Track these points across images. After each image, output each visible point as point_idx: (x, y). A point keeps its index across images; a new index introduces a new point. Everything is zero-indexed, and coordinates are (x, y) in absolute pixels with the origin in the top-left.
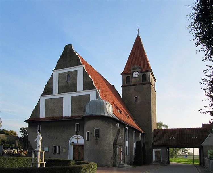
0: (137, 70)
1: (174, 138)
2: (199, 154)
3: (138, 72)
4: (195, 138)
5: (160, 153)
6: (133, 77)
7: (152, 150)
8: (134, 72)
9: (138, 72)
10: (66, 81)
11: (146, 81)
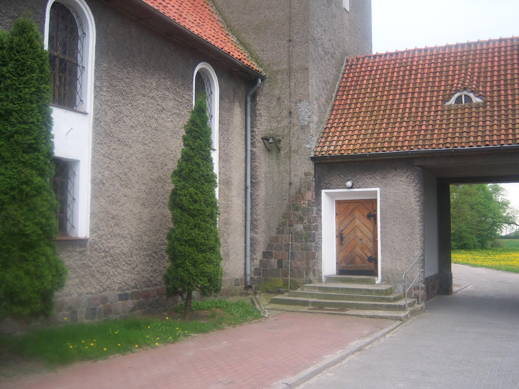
1: (476, 100)
2: (454, 196)
4: (468, 99)
5: (372, 217)
7: (309, 195)
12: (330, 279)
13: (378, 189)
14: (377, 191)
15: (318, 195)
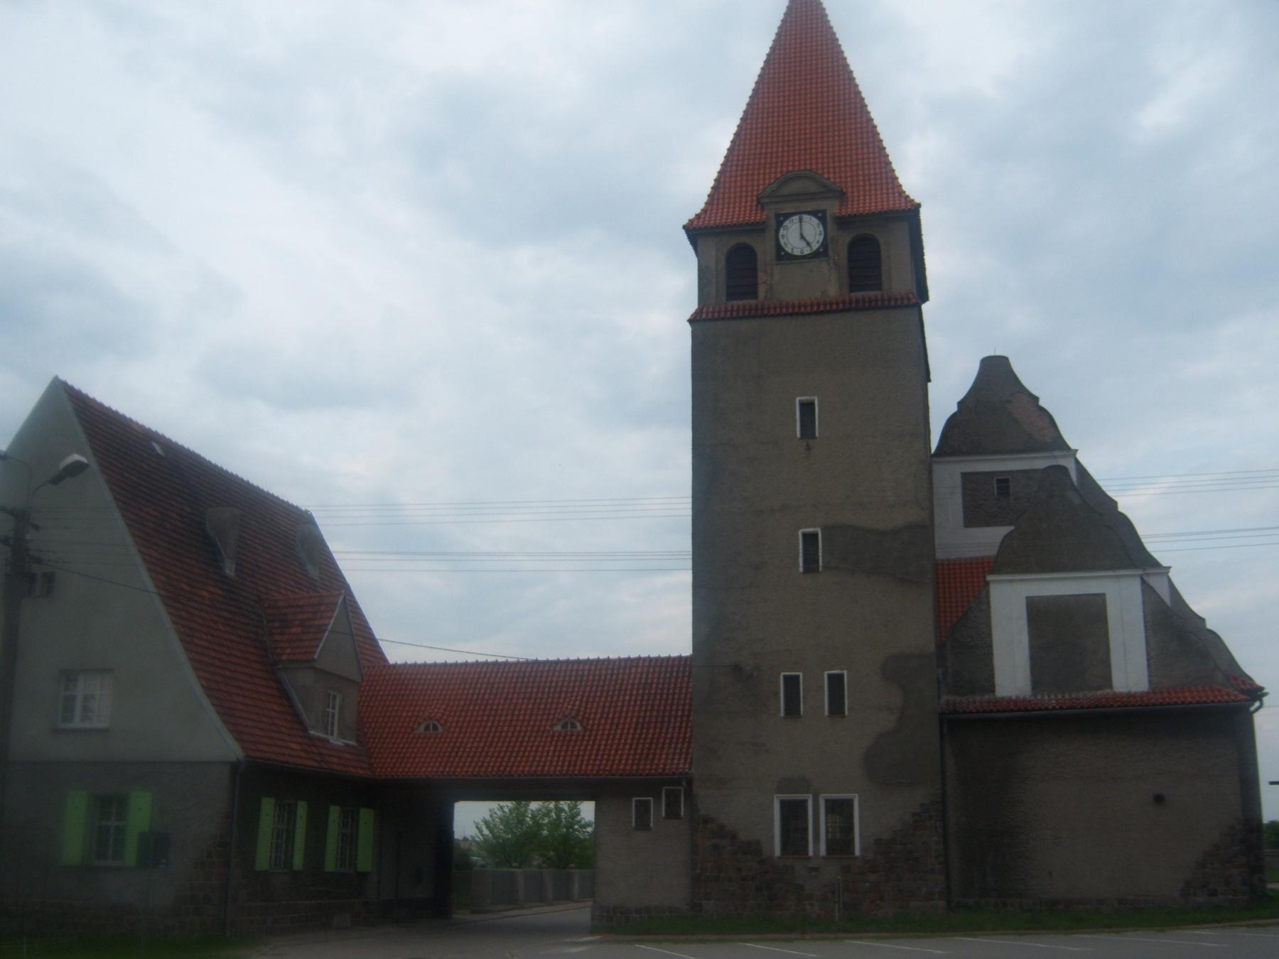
0: (811, 206)
3: (823, 220)
6: (782, 256)
8: (787, 216)
9: (820, 215)
11: (878, 286)
12: (779, 858)
13: (651, 799)
15: (773, 798)
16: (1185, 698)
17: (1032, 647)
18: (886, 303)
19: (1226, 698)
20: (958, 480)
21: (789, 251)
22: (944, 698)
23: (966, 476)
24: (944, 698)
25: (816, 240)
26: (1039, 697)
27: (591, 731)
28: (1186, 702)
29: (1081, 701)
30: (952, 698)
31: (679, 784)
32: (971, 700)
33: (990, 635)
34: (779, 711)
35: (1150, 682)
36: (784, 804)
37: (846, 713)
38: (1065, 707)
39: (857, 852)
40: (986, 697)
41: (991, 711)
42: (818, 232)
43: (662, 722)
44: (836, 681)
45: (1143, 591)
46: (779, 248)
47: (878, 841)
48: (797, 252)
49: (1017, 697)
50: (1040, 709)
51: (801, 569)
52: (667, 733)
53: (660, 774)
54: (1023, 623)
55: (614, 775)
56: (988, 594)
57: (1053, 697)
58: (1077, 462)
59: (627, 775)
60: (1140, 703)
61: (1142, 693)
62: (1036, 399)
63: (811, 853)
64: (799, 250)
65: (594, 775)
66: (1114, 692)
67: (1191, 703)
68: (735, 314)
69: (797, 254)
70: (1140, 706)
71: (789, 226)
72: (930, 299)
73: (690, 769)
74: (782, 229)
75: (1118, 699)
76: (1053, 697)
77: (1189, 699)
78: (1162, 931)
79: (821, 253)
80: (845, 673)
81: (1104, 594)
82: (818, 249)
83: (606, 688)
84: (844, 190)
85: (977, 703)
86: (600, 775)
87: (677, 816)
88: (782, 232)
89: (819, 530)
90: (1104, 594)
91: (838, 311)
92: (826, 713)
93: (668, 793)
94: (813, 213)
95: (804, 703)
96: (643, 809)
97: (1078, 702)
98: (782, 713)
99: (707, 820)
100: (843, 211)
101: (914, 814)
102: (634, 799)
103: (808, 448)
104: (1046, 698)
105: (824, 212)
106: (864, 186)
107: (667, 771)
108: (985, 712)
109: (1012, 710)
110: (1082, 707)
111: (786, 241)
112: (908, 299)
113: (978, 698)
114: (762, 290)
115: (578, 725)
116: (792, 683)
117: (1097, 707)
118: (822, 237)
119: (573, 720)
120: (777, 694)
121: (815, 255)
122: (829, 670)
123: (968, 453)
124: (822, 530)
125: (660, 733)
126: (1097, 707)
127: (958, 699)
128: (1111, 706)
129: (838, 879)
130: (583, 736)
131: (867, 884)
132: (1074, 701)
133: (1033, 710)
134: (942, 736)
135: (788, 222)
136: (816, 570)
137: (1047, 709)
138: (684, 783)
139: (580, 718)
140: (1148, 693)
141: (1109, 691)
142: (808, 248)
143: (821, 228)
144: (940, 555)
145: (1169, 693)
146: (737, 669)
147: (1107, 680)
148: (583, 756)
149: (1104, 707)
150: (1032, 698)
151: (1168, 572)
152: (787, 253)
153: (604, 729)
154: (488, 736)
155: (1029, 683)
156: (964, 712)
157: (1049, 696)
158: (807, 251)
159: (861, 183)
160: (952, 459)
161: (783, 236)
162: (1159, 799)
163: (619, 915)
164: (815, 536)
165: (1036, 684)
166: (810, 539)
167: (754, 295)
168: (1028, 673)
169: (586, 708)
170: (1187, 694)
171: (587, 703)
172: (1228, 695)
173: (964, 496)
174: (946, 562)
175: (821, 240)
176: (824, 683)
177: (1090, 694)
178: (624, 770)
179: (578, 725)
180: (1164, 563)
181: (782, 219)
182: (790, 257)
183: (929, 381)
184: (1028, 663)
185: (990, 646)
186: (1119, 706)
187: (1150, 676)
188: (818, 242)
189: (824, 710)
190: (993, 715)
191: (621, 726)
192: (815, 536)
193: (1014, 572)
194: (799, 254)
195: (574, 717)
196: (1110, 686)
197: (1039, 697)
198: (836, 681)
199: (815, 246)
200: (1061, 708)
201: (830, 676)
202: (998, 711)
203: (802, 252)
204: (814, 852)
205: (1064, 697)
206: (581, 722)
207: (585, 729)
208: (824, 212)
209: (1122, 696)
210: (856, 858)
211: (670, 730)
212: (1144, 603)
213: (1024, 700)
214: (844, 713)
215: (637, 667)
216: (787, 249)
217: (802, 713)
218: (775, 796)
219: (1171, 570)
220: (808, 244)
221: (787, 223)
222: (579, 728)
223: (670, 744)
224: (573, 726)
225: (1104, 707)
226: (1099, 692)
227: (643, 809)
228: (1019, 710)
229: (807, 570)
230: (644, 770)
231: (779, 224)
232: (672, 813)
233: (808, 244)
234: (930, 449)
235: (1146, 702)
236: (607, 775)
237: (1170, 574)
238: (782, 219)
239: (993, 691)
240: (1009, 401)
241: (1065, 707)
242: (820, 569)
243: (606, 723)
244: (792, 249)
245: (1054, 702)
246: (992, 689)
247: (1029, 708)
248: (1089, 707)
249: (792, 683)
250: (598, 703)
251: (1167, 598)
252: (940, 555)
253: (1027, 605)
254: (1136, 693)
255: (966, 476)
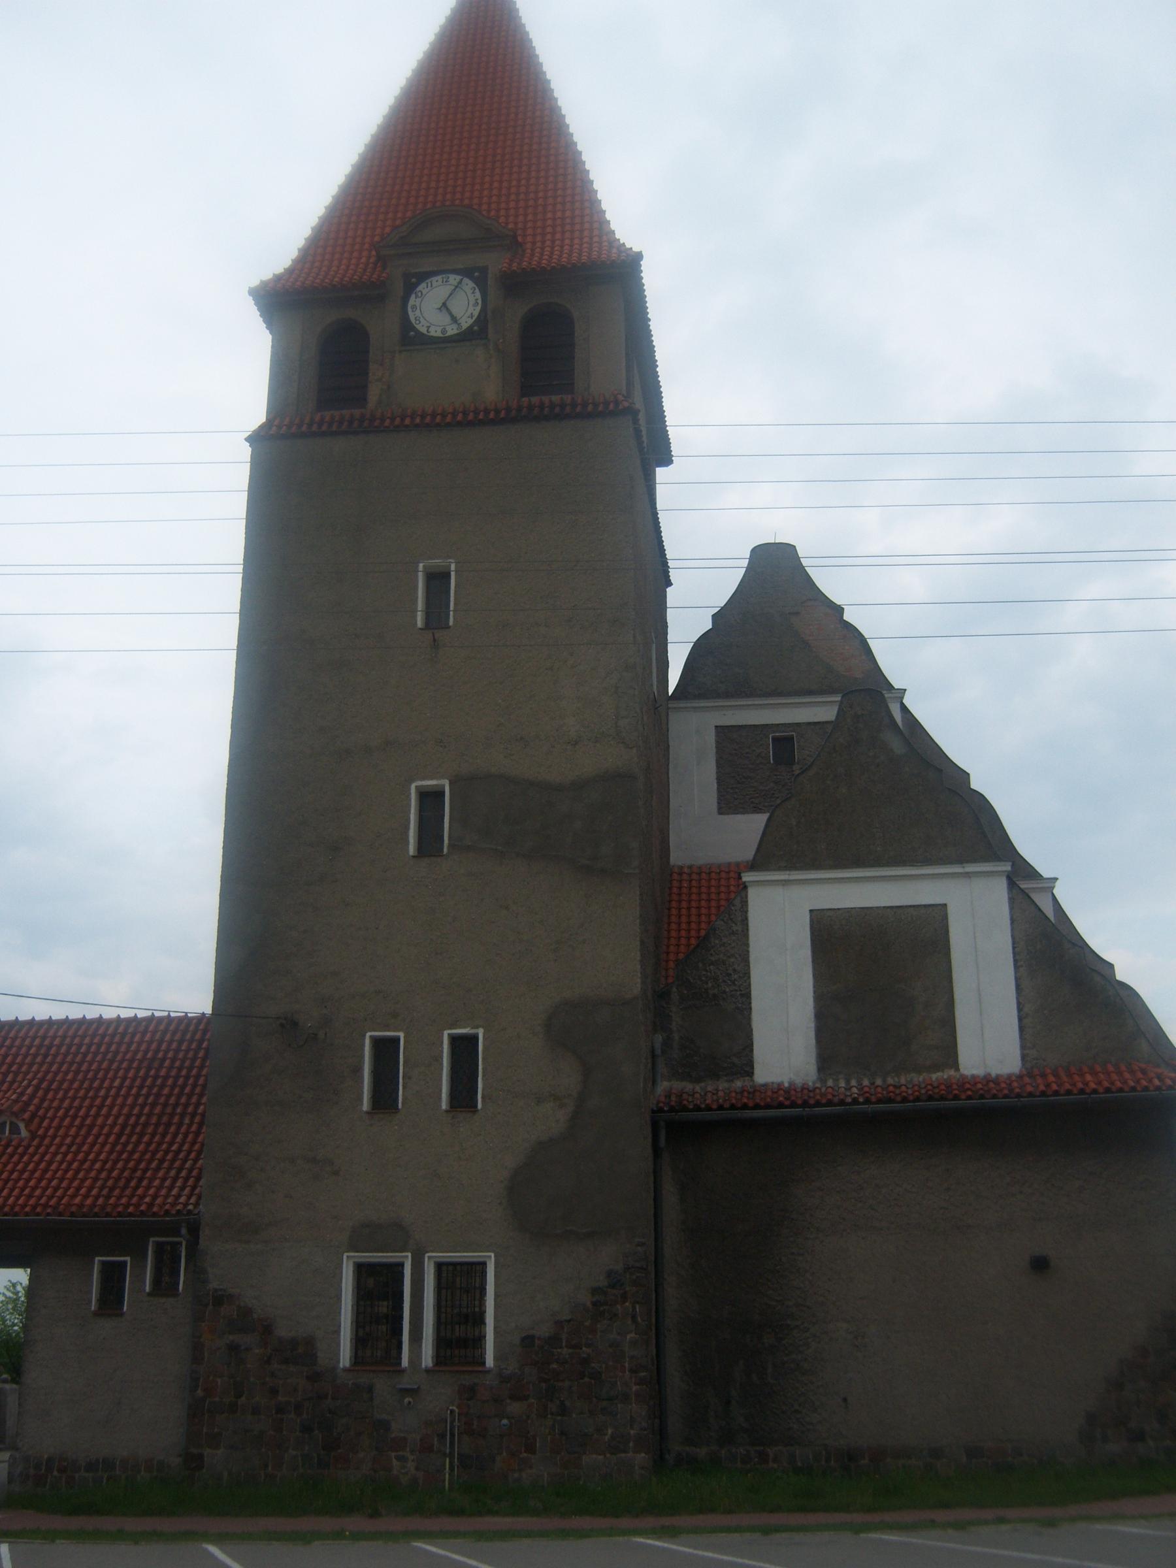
3: (481, 283)
6: (411, 338)
8: (424, 276)
9: (478, 276)
10: (420, 622)
12: (345, 1370)
13: (128, 1259)
14: (125, 1262)
16: (1087, 1084)
17: (819, 997)
18: (579, 409)
19: (1157, 1082)
20: (711, 738)
21: (423, 330)
22: (663, 1086)
23: (723, 732)
24: (663, 1086)
25: (469, 313)
26: (830, 1083)
27: (43, 1137)
28: (1088, 1091)
29: (903, 1088)
30: (678, 1085)
31: (177, 1233)
32: (709, 1089)
33: (747, 975)
34: (360, 1099)
35: (1024, 1057)
36: (362, 1270)
37: (480, 1106)
38: (873, 1099)
39: (490, 1361)
40: (738, 1084)
41: (745, 1107)
42: (472, 301)
43: (169, 1124)
44: (464, 1048)
45: (1012, 900)
46: (406, 325)
47: (528, 1341)
48: (435, 332)
49: (791, 1084)
50: (830, 1103)
51: (412, 850)
52: (171, 1144)
53: (143, 1213)
54: (805, 953)
55: (60, 1214)
56: (745, 903)
57: (854, 1083)
58: (904, 709)
59: (84, 1216)
60: (1006, 1092)
61: (1010, 1076)
62: (839, 610)
63: (405, 1362)
64: (439, 330)
65: (27, 1214)
66: (963, 1077)
67: (1095, 1091)
68: (324, 428)
69: (435, 335)
70: (1006, 1096)
71: (424, 292)
72: (676, 447)
73: (196, 1205)
74: (413, 296)
75: (968, 1086)
76: (854, 1083)
77: (1092, 1085)
78: (1051, 1523)
79: (475, 334)
80: (481, 1033)
81: (945, 905)
82: (471, 327)
83: (84, 1068)
84: (520, 239)
85: (721, 1094)
86: (38, 1214)
87: (172, 1290)
88: (412, 301)
89: (446, 784)
90: (945, 905)
91: (493, 422)
92: (444, 1105)
93: (160, 1249)
94: (467, 273)
95: (404, 1087)
96: (113, 1279)
97: (898, 1092)
98: (366, 1105)
99: (220, 1299)
100: (515, 264)
101: (595, 1291)
102: (97, 1259)
103: (435, 642)
104: (842, 1084)
105: (484, 270)
106: (553, 234)
107: (155, 1209)
108: (733, 1107)
109: (781, 1105)
110: (905, 1100)
111: (418, 305)
112: (617, 402)
113: (723, 1085)
114: (374, 393)
115: (22, 1126)
116: (385, 1050)
117: (930, 1098)
118: (478, 308)
119: (14, 1119)
120: (358, 1070)
121: (466, 337)
122: (450, 1029)
123: (728, 695)
124: (451, 784)
125: (160, 1144)
126: (930, 1098)
127: (688, 1086)
128: (956, 1098)
129: (452, 1411)
130: (27, 1147)
131: (505, 1421)
132: (891, 1088)
133: (818, 1104)
134: (657, 1152)
135: (423, 285)
136: (438, 853)
137: (842, 1103)
138: (184, 1231)
139: (26, 1115)
140: (1020, 1077)
141: (952, 1072)
142: (455, 326)
143: (478, 295)
144: (677, 857)
145: (1056, 1075)
146: (289, 1025)
147: (949, 1052)
148: (17, 1181)
149: (942, 1098)
150: (818, 1085)
151: (1053, 888)
152: (417, 284)
153: (66, 1135)
154: (74, 1178)
155: (813, 1060)
156: (698, 1109)
157: (848, 1081)
158: (452, 330)
159: (549, 229)
160: (703, 703)
161: (414, 307)
162: (1040, 1264)
163: (55, 1473)
164: (438, 794)
165: (826, 1060)
166: (430, 799)
167: (362, 400)
168: (813, 1041)
169: (43, 1100)
170: (1088, 1077)
171: (47, 1091)
172: (1159, 1077)
173: (719, 765)
174: (686, 870)
175: (476, 313)
176: (442, 1052)
177: (918, 1078)
178: (81, 1206)
179: (22, 1126)
180: (1046, 873)
181: (414, 280)
182: (424, 341)
183: (669, 584)
184: (812, 1025)
185: (748, 996)
186: (969, 1098)
187: (1023, 1047)
188: (472, 316)
189: (440, 1098)
190: (748, 1114)
191: (95, 1131)
192: (438, 794)
193: (791, 866)
194: (439, 334)
195: (15, 1114)
196: (955, 1065)
197: (830, 1083)
198: (464, 1048)
199: (466, 323)
200: (867, 1101)
201: (454, 1039)
202: (757, 1107)
203: (444, 331)
204: (411, 1361)
205: (873, 1084)
206: (28, 1123)
207: (33, 1135)
208: (484, 270)
209: (975, 1080)
210: (489, 1371)
211: (179, 1138)
212: (1013, 921)
213: (804, 1088)
214: (476, 1106)
215: (144, 1033)
216: (418, 327)
217: (400, 1106)
218: (345, 1255)
219: (1058, 884)
220: (454, 319)
221: (422, 287)
222: (24, 1133)
223: (174, 1160)
224: (15, 1129)
225: (942, 1098)
226: (934, 1076)
227: (113, 1279)
228: (793, 1105)
229: (422, 851)
230: (115, 1206)
231: (410, 288)
232: (164, 1286)
233: (454, 319)
234: (668, 693)
235: (1017, 1090)
236: (48, 1214)
237: (1055, 891)
238: (414, 280)
239: (750, 1074)
240: (797, 613)
241: (873, 1099)
242: (445, 850)
243: (71, 1126)
244: (429, 327)
245: (855, 1090)
246: (747, 1069)
247: (812, 1102)
248: (917, 1099)
249: (385, 1050)
250: (67, 1091)
251: (1049, 912)
252: (677, 857)
253: (812, 921)
254: (998, 1076)
255: (723, 732)
